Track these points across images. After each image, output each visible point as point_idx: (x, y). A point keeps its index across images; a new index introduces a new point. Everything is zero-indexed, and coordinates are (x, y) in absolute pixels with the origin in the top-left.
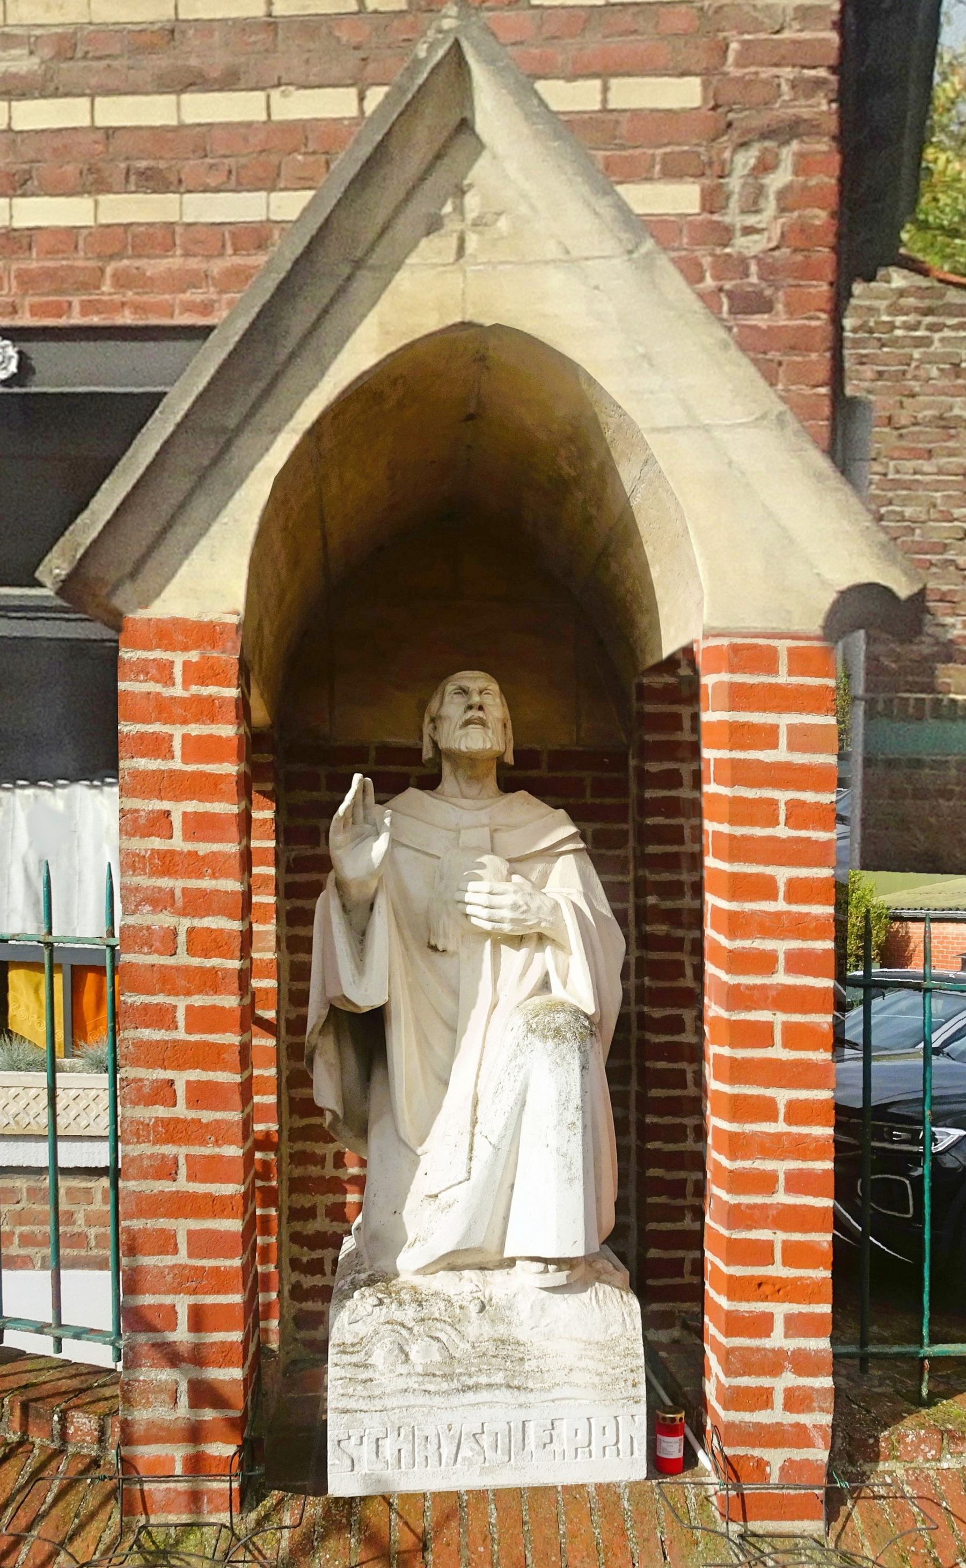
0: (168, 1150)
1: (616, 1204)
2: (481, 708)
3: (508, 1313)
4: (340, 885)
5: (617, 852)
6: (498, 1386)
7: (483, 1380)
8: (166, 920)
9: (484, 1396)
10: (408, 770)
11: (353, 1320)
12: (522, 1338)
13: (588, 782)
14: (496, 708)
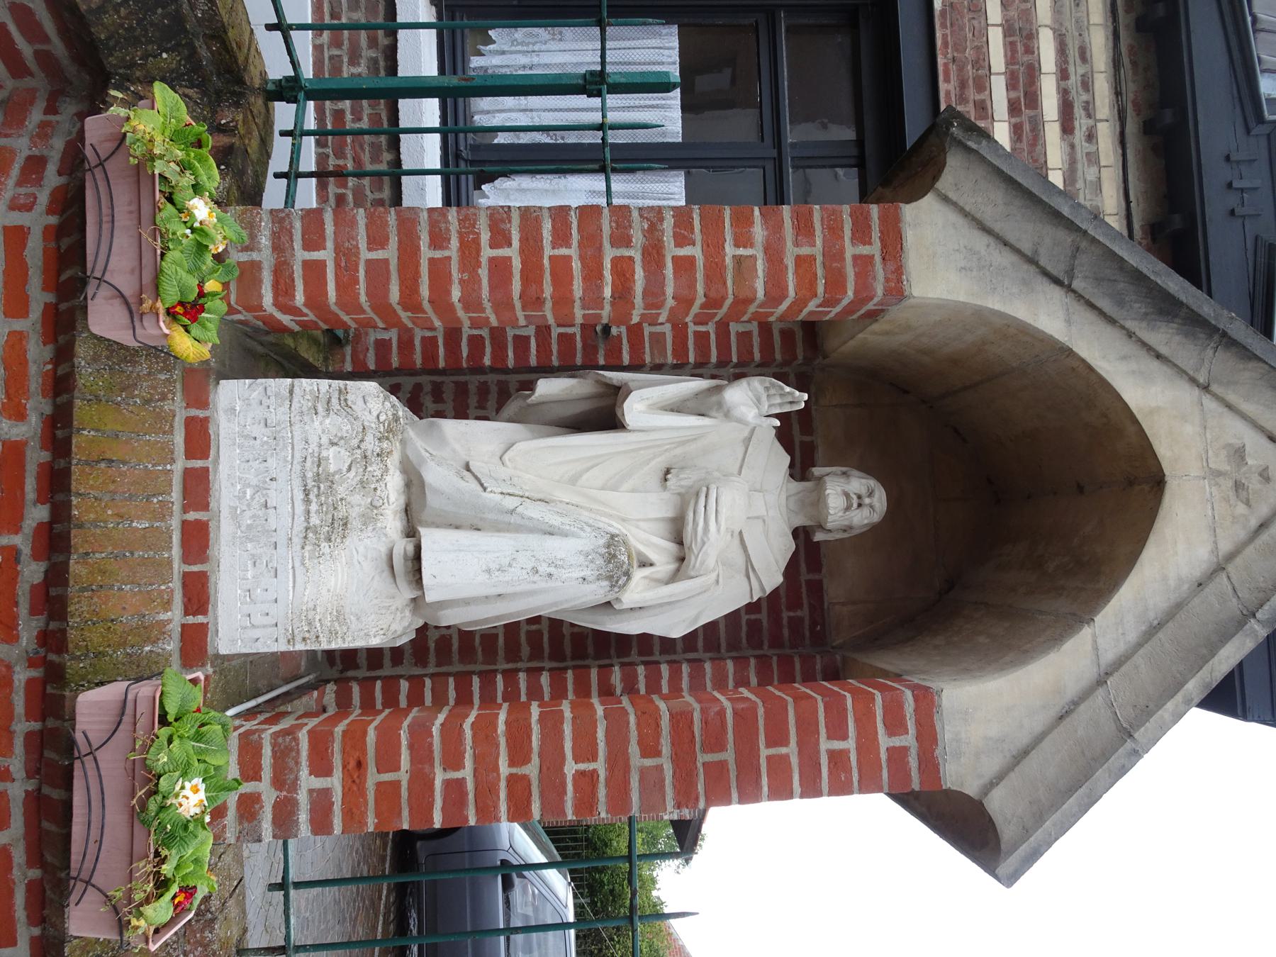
0: (455, 243)
1: (644, 634)
2: (860, 505)
3: (370, 528)
4: (719, 389)
5: (744, 641)
6: (307, 519)
7: (314, 507)
8: (638, 238)
9: (300, 508)
10: (802, 444)
11: (370, 400)
12: (347, 541)
13: (799, 613)
14: (862, 518)
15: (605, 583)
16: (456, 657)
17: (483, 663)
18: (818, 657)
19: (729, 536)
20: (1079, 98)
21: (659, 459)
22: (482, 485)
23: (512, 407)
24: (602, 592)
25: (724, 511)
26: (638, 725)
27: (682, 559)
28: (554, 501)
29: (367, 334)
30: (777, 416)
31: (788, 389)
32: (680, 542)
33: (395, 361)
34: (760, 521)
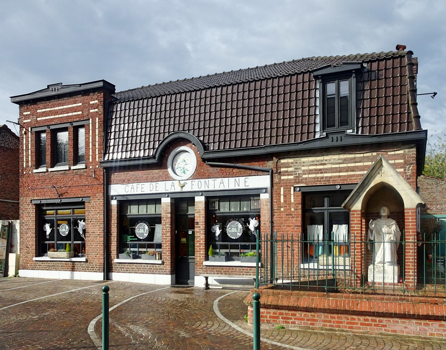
20: (320, 162)
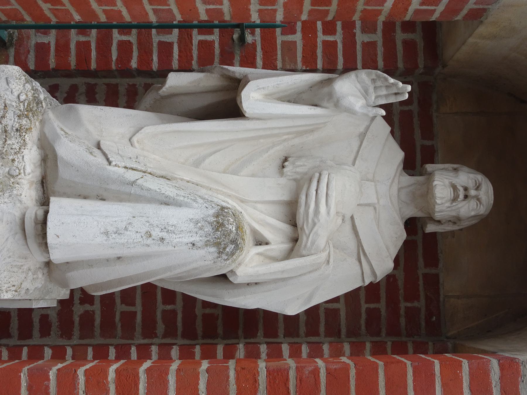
2: (466, 197)
3: (7, 195)
4: (330, 81)
5: (363, 328)
13: (416, 304)
15: (213, 249)
16: (97, 331)
17: (122, 338)
18: (430, 344)
19: (340, 221)
21: (278, 148)
22: (108, 159)
23: (149, 98)
24: (210, 257)
25: (333, 194)
26: (237, 379)
27: (295, 240)
28: (175, 179)
29: (29, 38)
30: (381, 106)
31: (392, 80)
32: (294, 225)
33: (52, 63)
34: (372, 208)
